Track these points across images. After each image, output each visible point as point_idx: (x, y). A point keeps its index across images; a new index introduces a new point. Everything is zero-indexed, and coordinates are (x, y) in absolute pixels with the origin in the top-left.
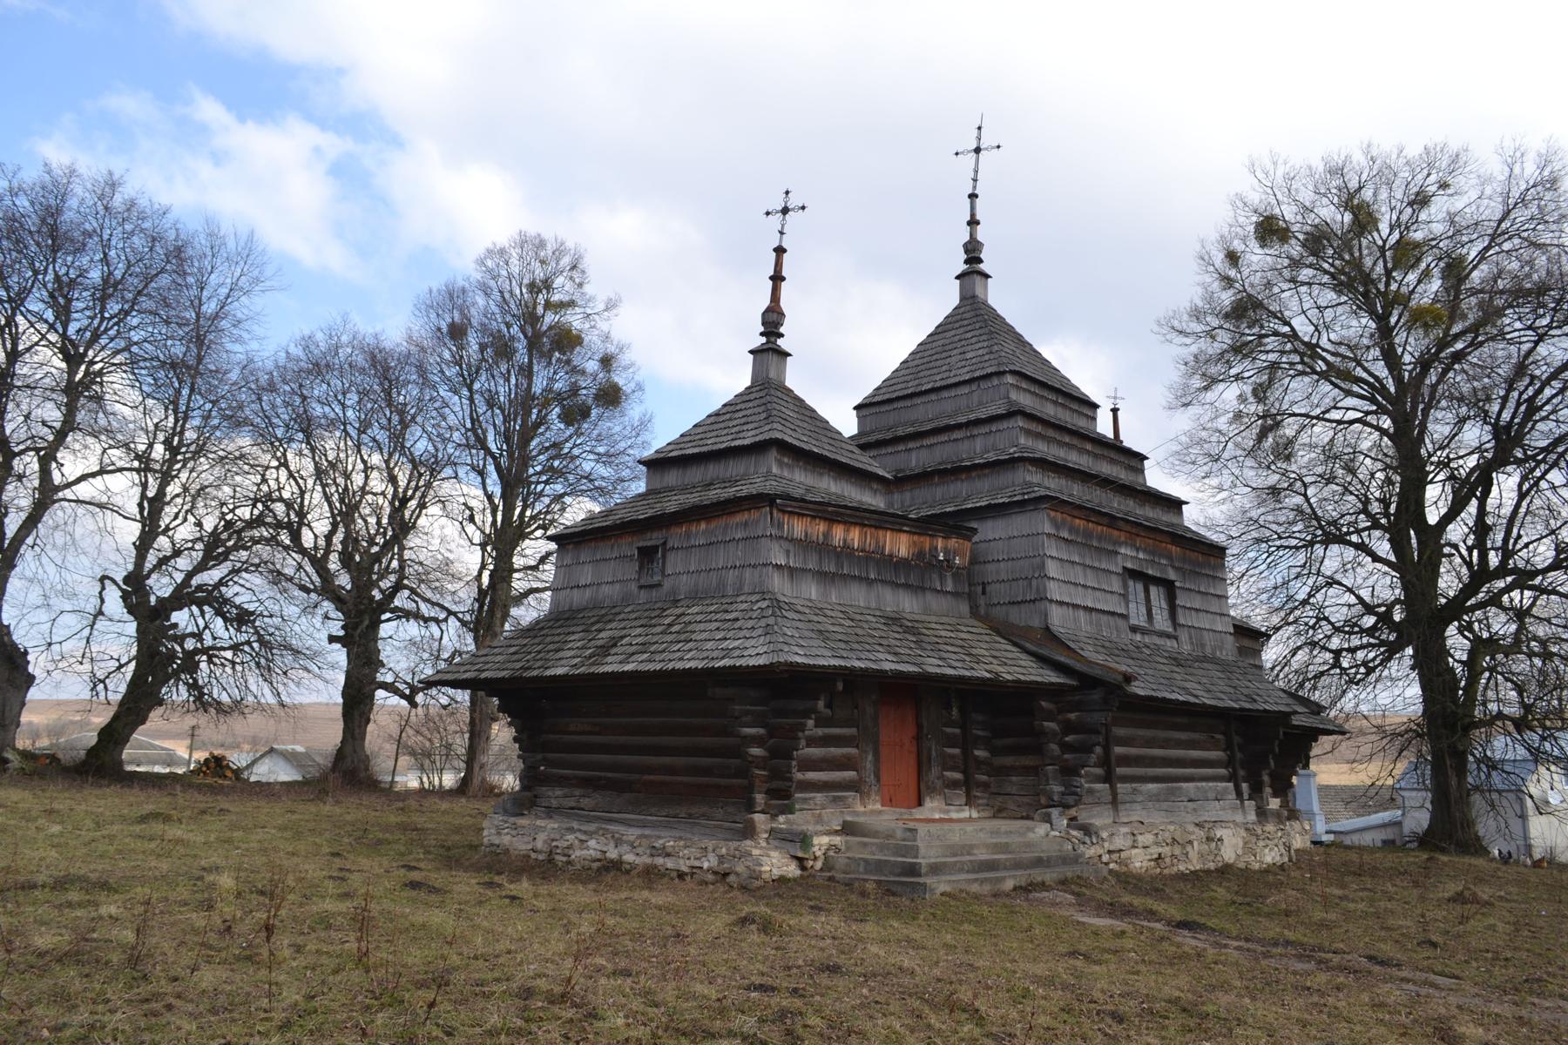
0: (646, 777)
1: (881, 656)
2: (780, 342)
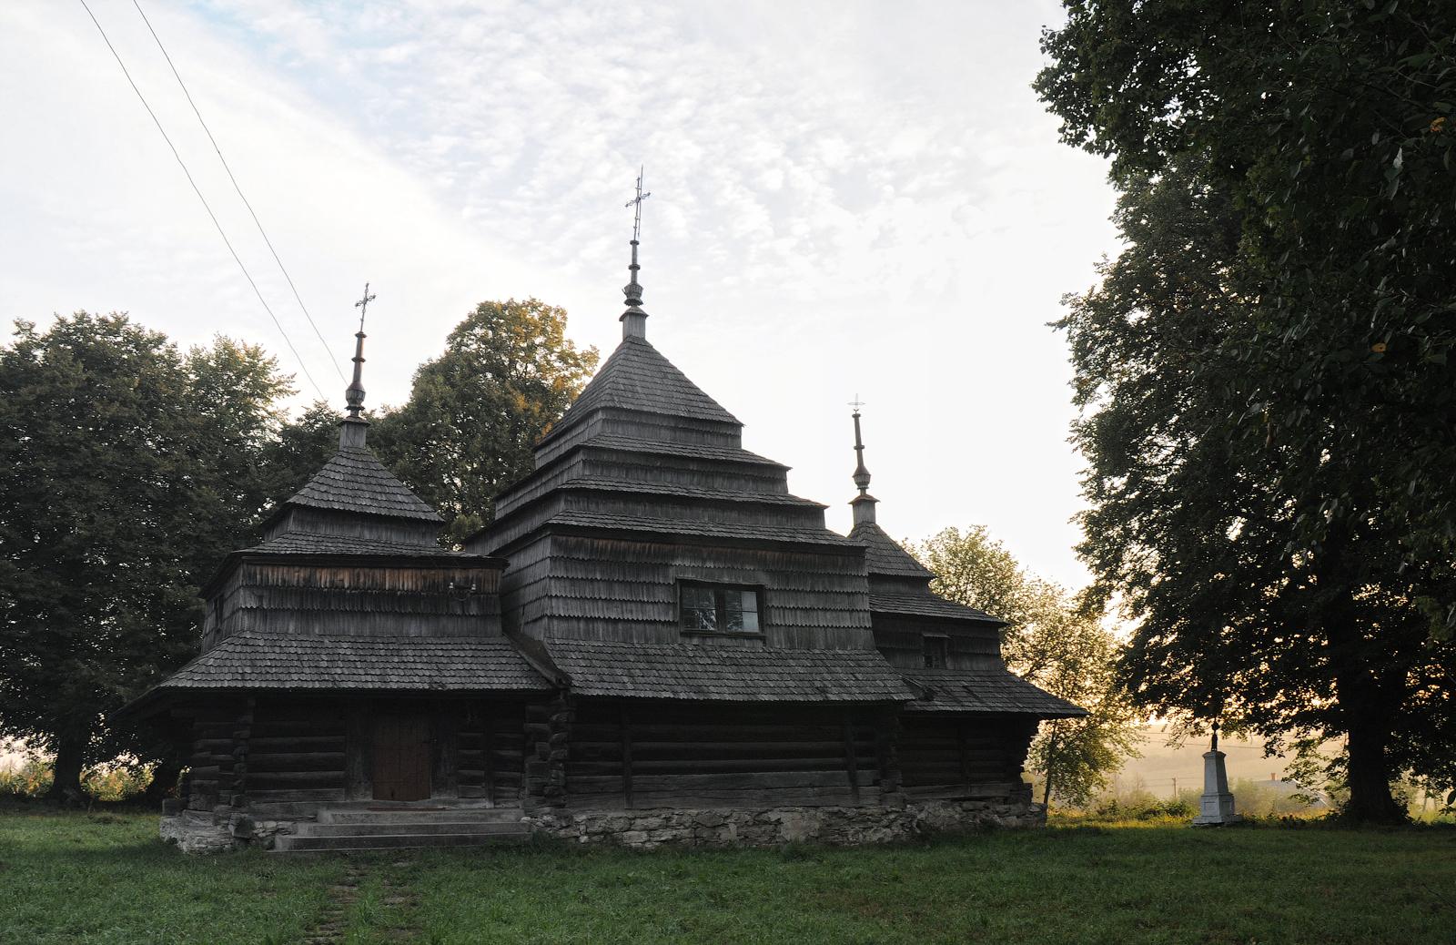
2: (640, 307)
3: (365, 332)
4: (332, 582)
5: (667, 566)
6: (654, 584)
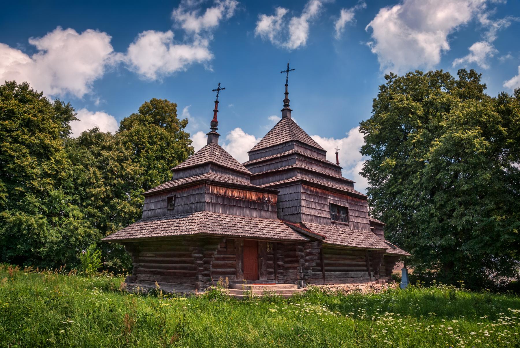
0: (169, 271)
1: (238, 231)
2: (216, 131)
4: (232, 194)
5: (327, 198)
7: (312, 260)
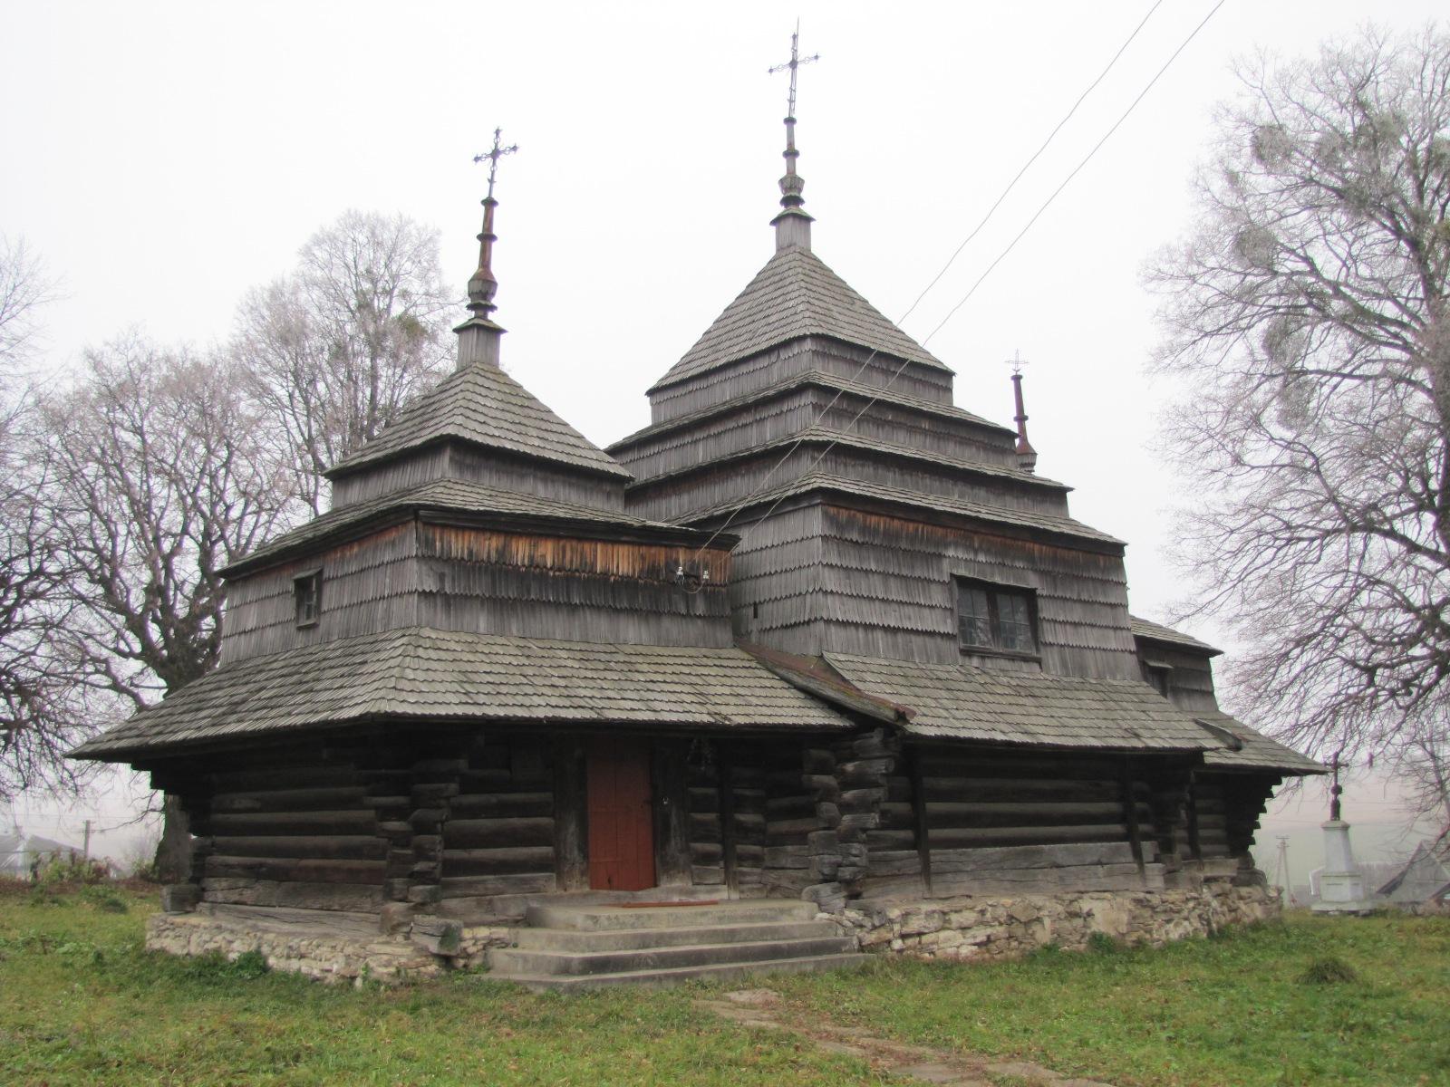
2: (491, 316)
3: (495, 196)
4: (531, 558)
5: (940, 556)
6: (929, 581)
7: (867, 806)
